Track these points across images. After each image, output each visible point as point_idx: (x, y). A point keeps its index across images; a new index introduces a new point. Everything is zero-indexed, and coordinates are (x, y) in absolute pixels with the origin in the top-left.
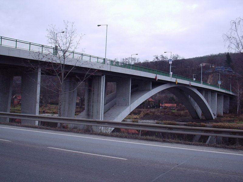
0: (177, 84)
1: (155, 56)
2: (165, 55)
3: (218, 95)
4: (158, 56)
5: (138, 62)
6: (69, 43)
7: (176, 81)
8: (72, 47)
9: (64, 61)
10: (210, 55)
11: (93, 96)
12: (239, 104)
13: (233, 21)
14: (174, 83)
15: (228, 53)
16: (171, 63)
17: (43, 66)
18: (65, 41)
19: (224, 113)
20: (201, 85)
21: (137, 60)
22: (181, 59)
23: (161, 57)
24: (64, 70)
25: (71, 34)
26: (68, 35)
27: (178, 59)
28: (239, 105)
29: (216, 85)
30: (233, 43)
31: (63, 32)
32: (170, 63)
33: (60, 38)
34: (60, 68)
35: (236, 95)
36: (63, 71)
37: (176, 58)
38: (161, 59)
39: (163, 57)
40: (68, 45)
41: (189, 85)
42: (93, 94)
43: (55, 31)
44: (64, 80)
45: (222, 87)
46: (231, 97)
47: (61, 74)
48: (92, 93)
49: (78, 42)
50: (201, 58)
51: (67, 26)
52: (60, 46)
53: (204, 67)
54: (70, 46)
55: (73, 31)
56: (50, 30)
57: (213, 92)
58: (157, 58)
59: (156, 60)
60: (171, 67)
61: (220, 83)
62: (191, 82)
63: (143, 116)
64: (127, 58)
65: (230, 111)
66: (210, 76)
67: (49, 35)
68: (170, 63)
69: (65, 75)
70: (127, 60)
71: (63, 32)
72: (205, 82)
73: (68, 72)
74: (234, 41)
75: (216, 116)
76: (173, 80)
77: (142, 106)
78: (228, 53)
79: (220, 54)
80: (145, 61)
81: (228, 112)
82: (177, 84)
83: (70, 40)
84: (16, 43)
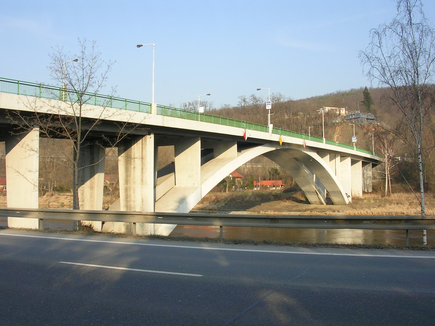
0: (281, 144)
1: (241, 97)
2: (258, 95)
3: (364, 164)
4: (246, 98)
5: (211, 109)
6: (87, 78)
7: (280, 139)
8: (93, 85)
9: (81, 109)
10: (336, 92)
11: (134, 171)
12: (388, 174)
13: (375, 30)
14: (278, 143)
15: (366, 87)
16: (269, 107)
17: (43, 120)
18: (80, 74)
19: (364, 192)
20: (323, 145)
21: (209, 105)
22: (286, 100)
23: (251, 98)
24: (80, 125)
25: (91, 60)
26: (86, 64)
27: (282, 100)
28: (388, 177)
29: (349, 144)
30: (376, 67)
31: (76, 60)
32: (267, 108)
33: (73, 70)
34: (73, 124)
35: (381, 160)
36: (79, 128)
37: (279, 99)
38: (251, 102)
39: (254, 98)
40: (86, 81)
41: (279, 142)
42: (134, 168)
43: (63, 58)
44: (81, 145)
45: (359, 146)
46: (375, 163)
47: (75, 133)
48: (132, 166)
49: (103, 75)
50: (321, 98)
51: (83, 48)
52: (73, 84)
53: (327, 114)
54: (91, 83)
55: (94, 57)
56: (54, 56)
57: (343, 156)
58: (244, 100)
59: (243, 104)
60: (269, 115)
61: (354, 140)
62: (305, 140)
63: (223, 205)
64: (191, 102)
65: (373, 189)
66: (338, 129)
67: (52, 65)
68: (267, 108)
69: (83, 133)
70: (192, 106)
71: (76, 60)
72: (330, 139)
73: (87, 131)
74: (378, 65)
75: (350, 199)
76: (275, 138)
77: (222, 186)
78: (366, 87)
79: (352, 90)
80: (224, 106)
81: (370, 190)
82: (281, 144)
83: (89, 72)
84: (139, 105)
